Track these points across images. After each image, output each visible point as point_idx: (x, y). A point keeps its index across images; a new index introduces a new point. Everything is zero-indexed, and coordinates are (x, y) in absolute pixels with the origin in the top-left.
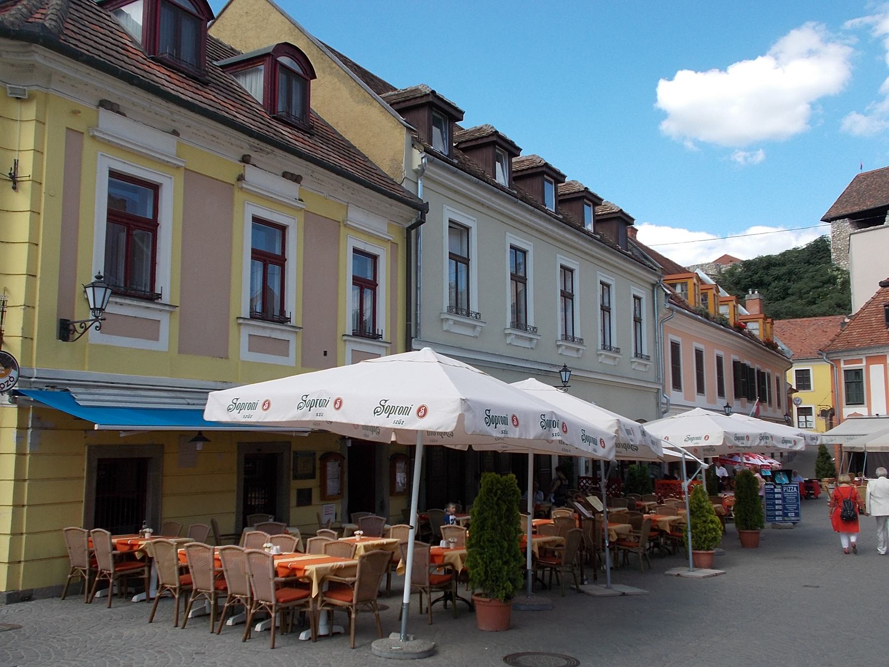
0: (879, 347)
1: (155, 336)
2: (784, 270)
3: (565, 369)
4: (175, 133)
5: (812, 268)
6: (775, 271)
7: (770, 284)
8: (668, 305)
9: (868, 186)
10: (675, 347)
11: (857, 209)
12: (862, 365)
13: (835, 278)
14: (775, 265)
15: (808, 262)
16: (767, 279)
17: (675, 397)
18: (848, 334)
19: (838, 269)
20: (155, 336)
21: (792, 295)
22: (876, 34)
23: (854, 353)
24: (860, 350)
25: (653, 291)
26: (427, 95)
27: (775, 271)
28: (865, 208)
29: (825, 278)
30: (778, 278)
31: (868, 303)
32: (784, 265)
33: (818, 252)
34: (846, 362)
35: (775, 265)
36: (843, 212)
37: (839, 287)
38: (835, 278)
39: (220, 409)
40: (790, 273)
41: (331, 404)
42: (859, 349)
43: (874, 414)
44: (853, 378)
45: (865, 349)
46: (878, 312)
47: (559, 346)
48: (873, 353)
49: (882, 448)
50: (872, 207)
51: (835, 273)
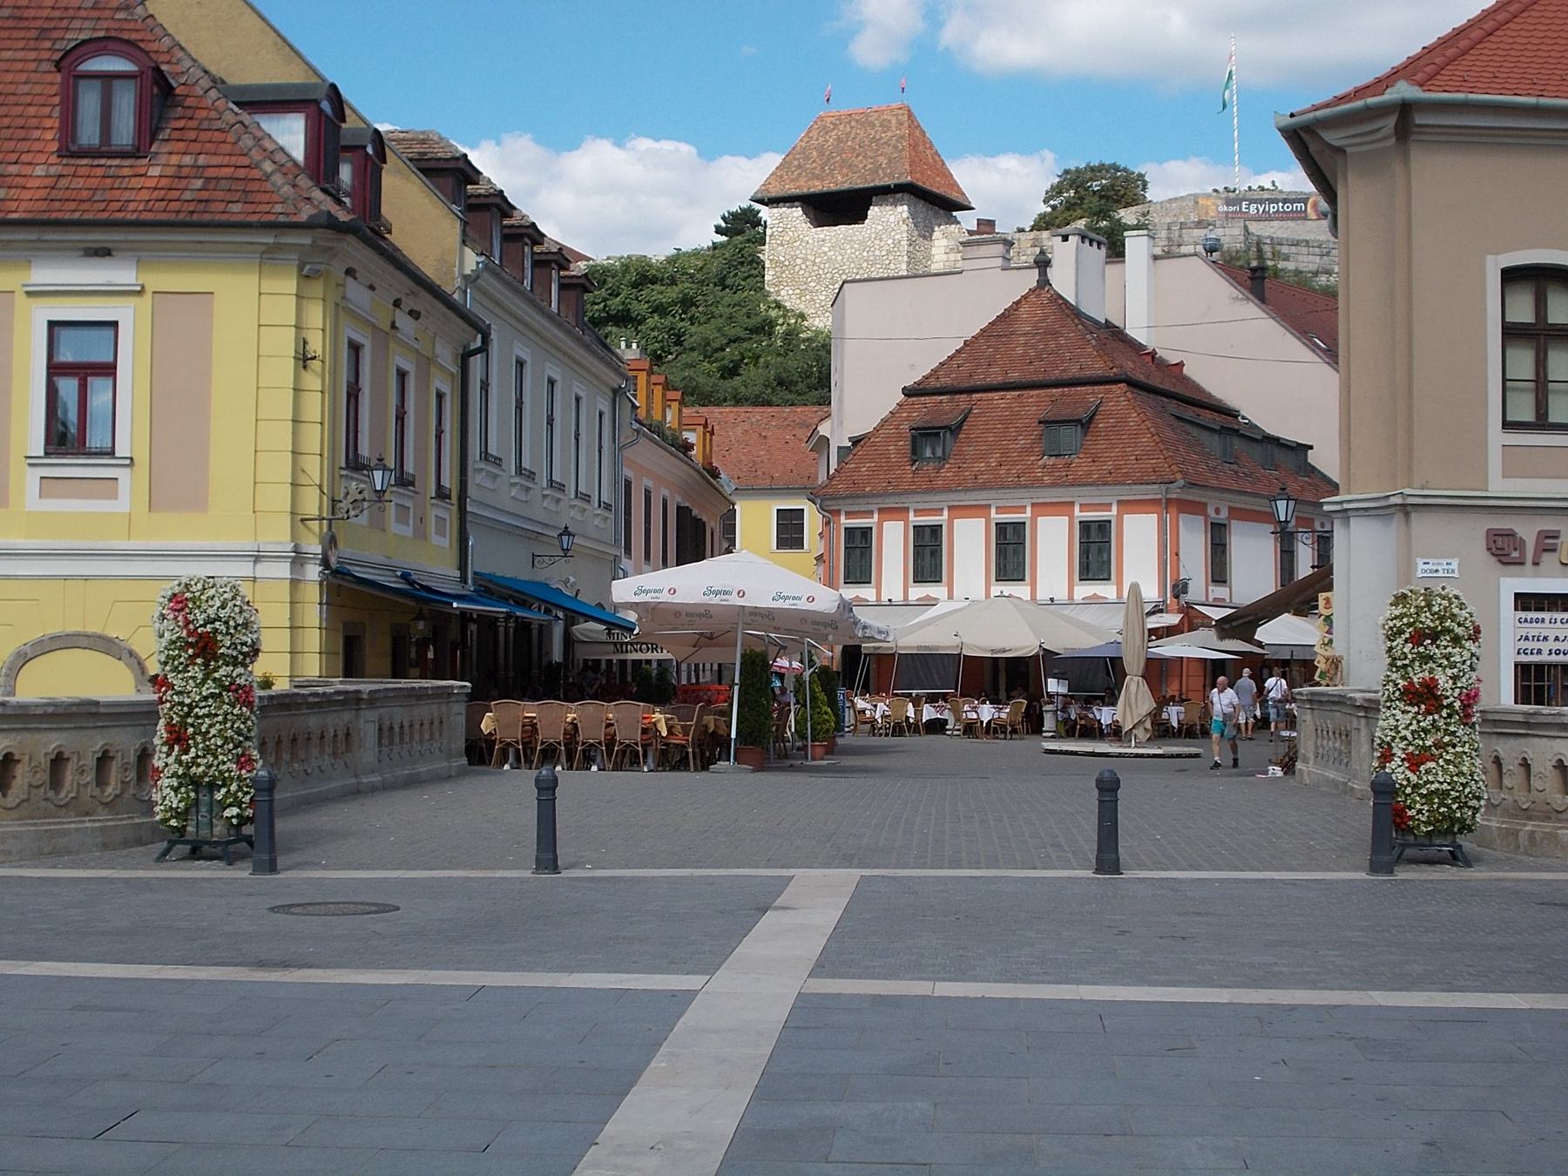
0: (900, 494)
1: (113, 495)
2: (673, 293)
3: (566, 532)
4: (372, 288)
5: (728, 297)
6: (657, 294)
7: (642, 321)
8: (636, 426)
9: (839, 140)
10: (628, 484)
11: (818, 187)
12: (871, 521)
13: (772, 323)
14: (654, 281)
15: (722, 283)
16: (639, 308)
17: (626, 563)
18: (857, 470)
19: (779, 306)
20: (113, 495)
21: (693, 349)
22: (940, 48)
23: (861, 501)
24: (874, 496)
25: (614, 401)
26: (457, 159)
27: (657, 294)
28: (833, 187)
29: (753, 322)
30: (660, 310)
31: (884, 421)
32: (673, 282)
33: (742, 263)
34: (849, 514)
35: (654, 281)
36: (792, 189)
37: (779, 343)
38: (772, 323)
39: (624, 590)
40: (687, 303)
41: (735, 593)
42: (871, 495)
43: (884, 599)
44: (858, 542)
45: (878, 495)
46: (900, 437)
47: (545, 496)
48: (890, 503)
49: (919, 648)
50: (846, 186)
51: (773, 313)
